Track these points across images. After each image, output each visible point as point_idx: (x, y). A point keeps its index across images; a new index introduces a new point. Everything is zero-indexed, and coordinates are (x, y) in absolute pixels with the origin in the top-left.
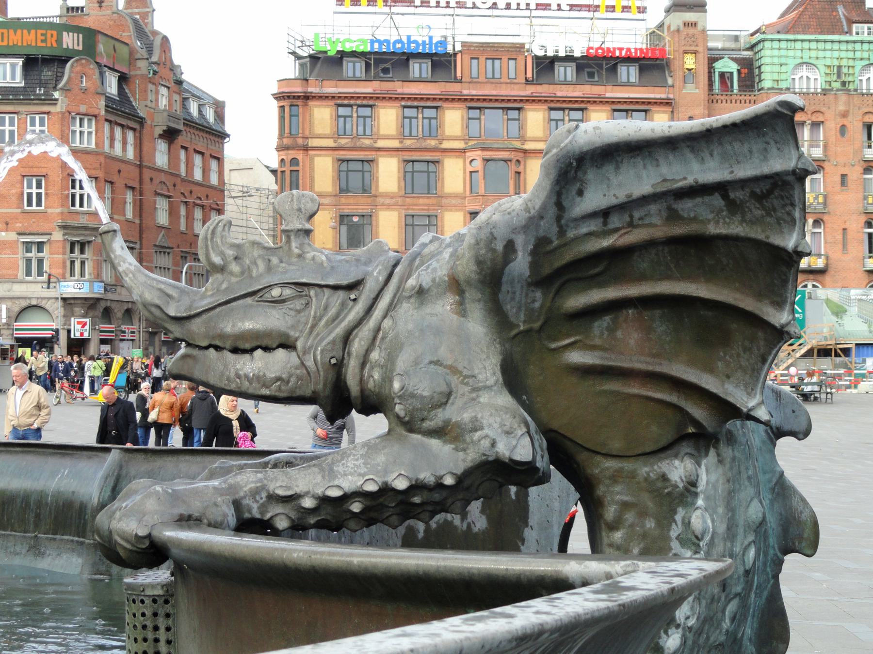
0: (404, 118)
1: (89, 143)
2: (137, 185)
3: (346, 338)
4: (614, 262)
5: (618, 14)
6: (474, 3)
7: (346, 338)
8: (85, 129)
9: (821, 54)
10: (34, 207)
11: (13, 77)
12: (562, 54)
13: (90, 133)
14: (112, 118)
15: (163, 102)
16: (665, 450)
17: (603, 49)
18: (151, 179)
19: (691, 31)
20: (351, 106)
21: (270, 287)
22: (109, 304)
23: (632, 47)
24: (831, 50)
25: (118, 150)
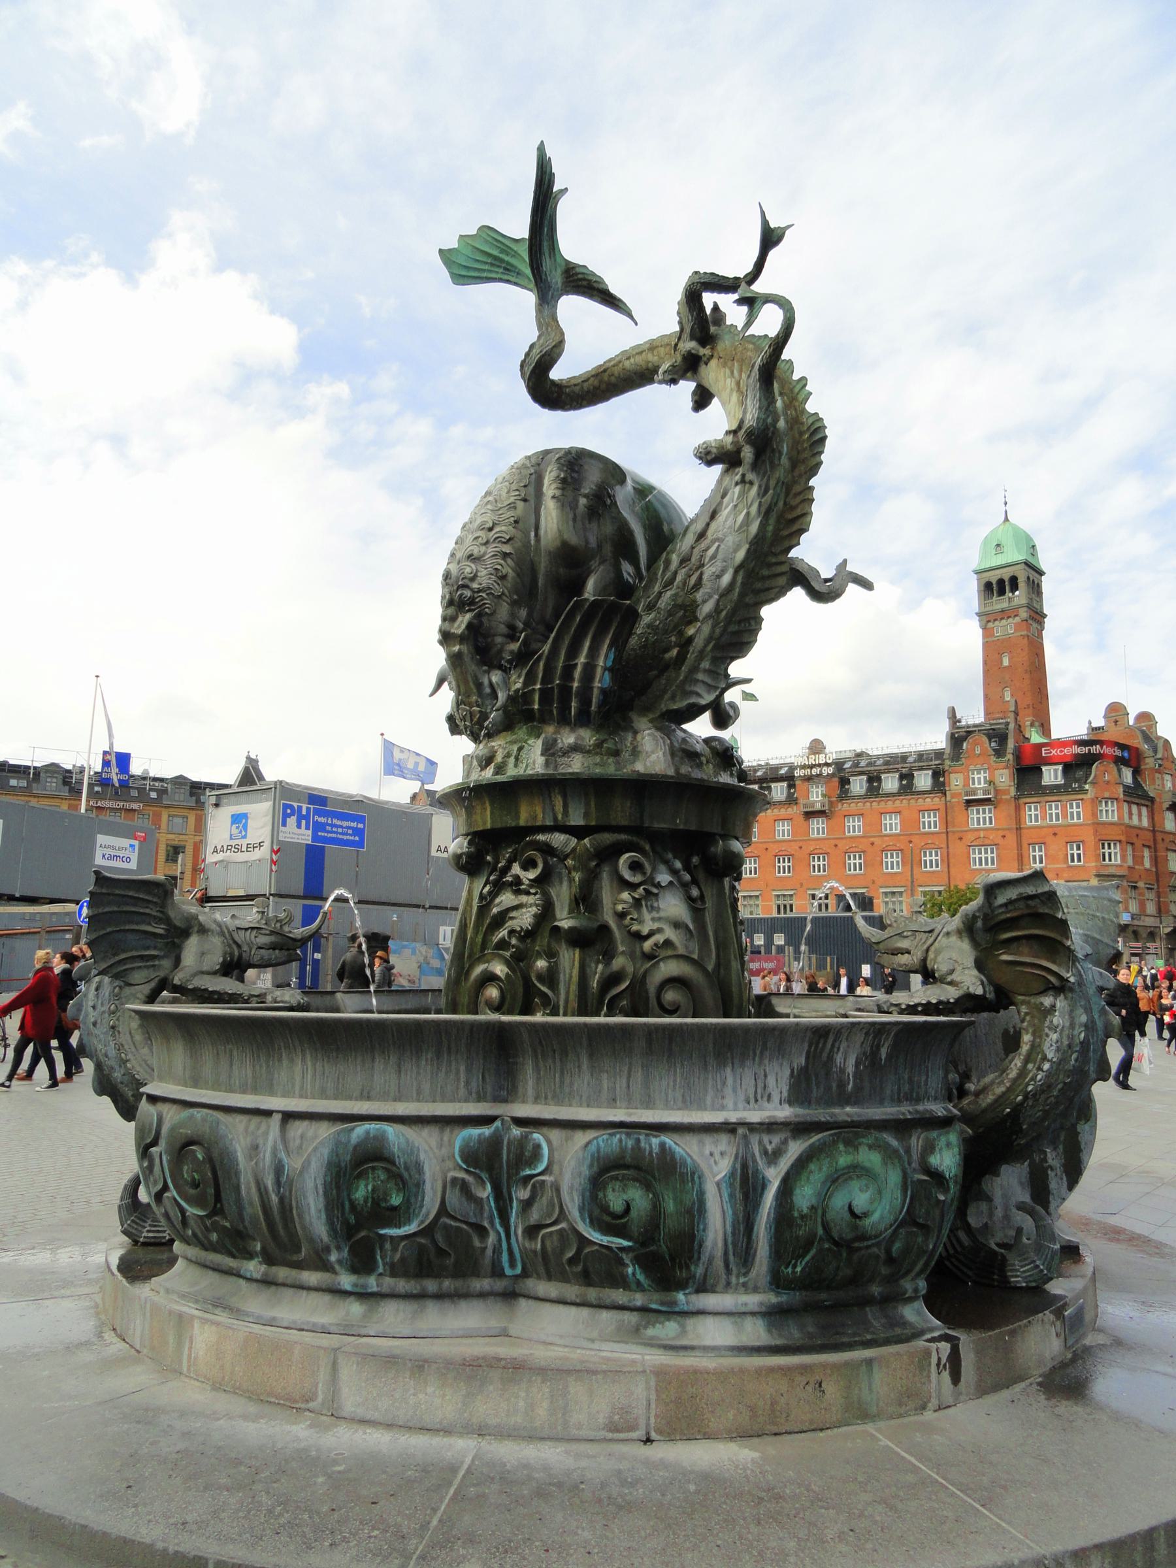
1: (1113, 816)
2: (1151, 844)
3: (927, 950)
4: (1011, 923)
7: (927, 950)
10: (1076, 863)
11: (1056, 778)
14: (1129, 799)
16: (1043, 992)
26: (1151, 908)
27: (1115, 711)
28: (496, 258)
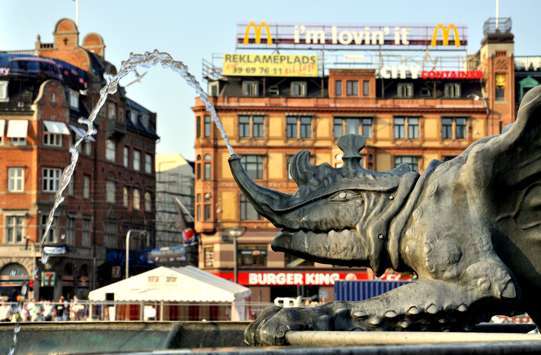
0: (288, 124)
1: (57, 143)
5: (445, 46)
6: (338, 41)
12: (403, 76)
17: (434, 73)
18: (103, 170)
19: (502, 58)
20: (249, 116)
21: (338, 192)
22: (70, 261)
23: (456, 70)
26: (86, 240)
27: (64, 27)
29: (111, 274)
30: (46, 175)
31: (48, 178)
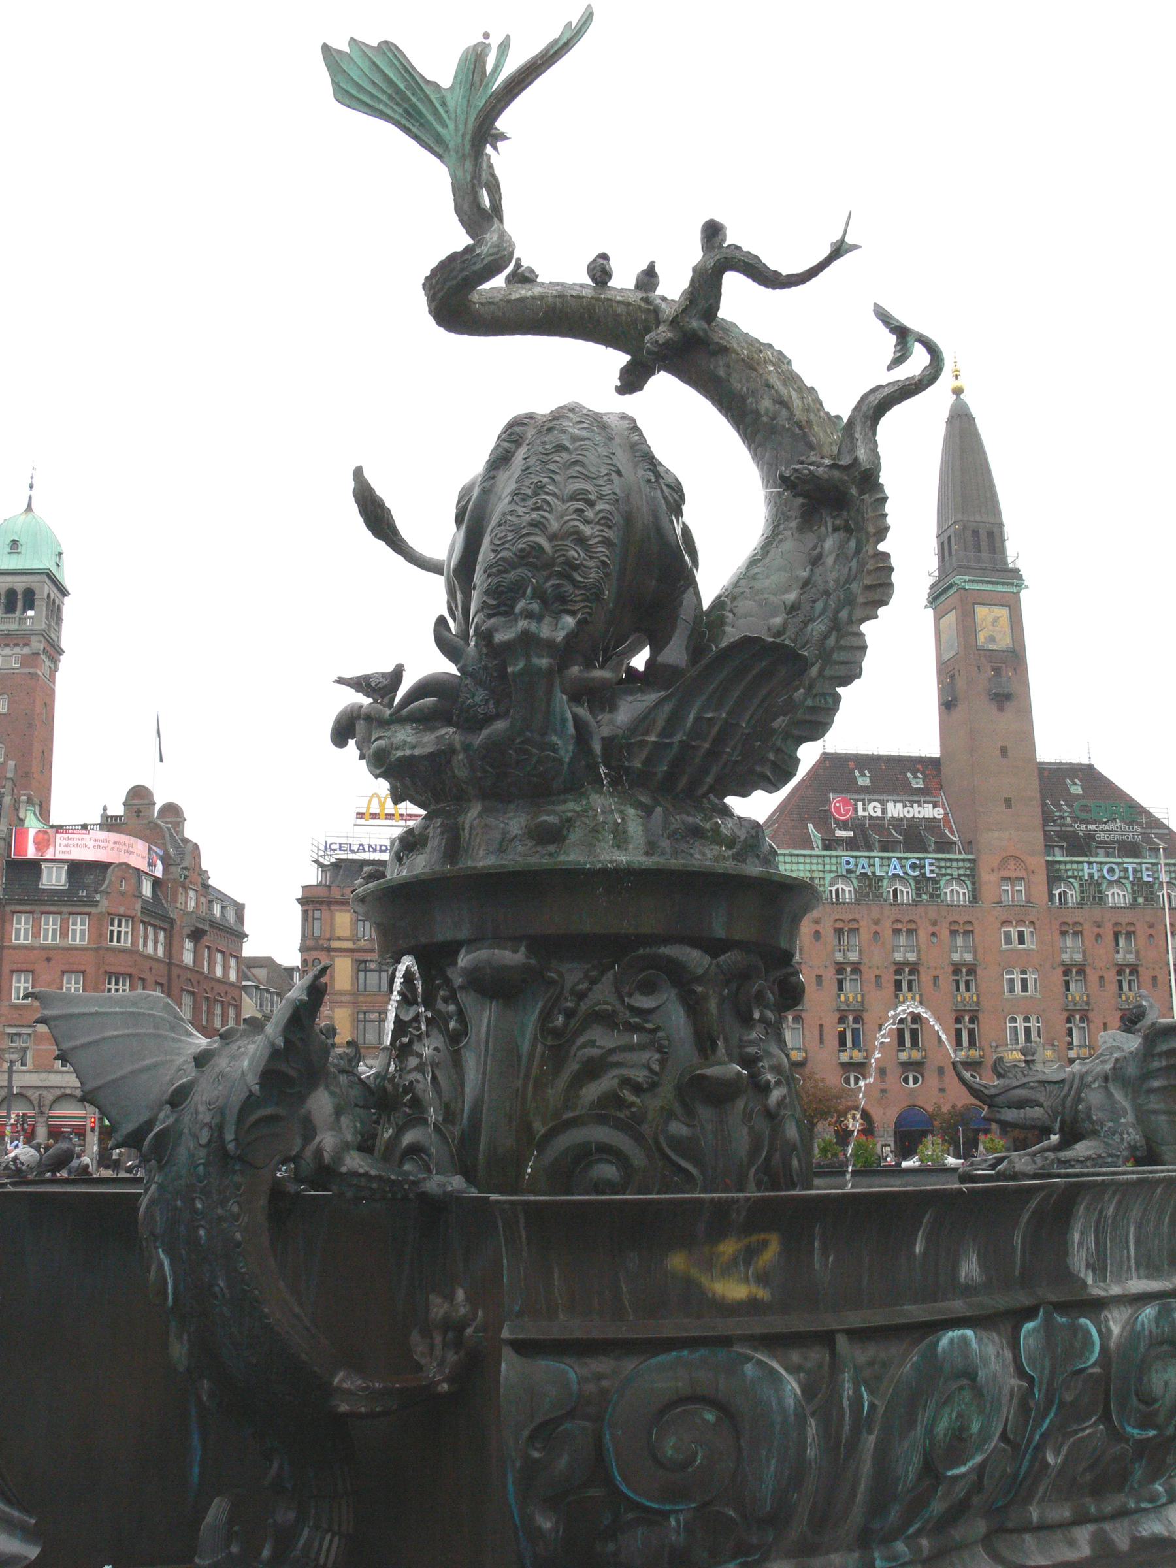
1: (126, 941)
8: (123, 929)
9: (795, 867)
13: (126, 933)
15: (192, 905)
18: (179, 976)
24: (804, 863)
25: (150, 949)
28: (398, 90)
29: (260, 1554)
30: (112, 925)
31: (116, 928)
